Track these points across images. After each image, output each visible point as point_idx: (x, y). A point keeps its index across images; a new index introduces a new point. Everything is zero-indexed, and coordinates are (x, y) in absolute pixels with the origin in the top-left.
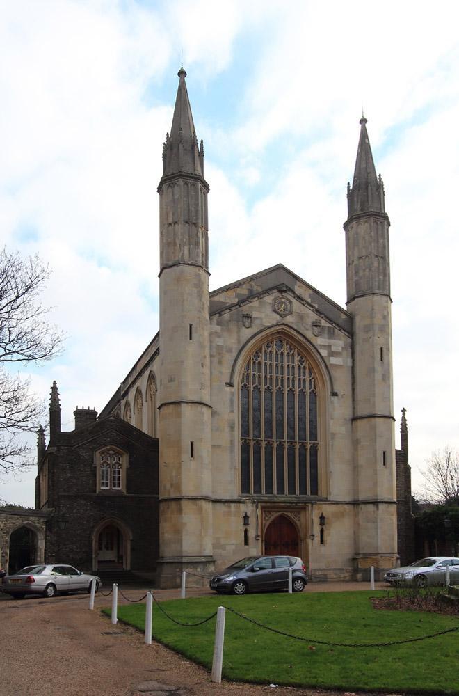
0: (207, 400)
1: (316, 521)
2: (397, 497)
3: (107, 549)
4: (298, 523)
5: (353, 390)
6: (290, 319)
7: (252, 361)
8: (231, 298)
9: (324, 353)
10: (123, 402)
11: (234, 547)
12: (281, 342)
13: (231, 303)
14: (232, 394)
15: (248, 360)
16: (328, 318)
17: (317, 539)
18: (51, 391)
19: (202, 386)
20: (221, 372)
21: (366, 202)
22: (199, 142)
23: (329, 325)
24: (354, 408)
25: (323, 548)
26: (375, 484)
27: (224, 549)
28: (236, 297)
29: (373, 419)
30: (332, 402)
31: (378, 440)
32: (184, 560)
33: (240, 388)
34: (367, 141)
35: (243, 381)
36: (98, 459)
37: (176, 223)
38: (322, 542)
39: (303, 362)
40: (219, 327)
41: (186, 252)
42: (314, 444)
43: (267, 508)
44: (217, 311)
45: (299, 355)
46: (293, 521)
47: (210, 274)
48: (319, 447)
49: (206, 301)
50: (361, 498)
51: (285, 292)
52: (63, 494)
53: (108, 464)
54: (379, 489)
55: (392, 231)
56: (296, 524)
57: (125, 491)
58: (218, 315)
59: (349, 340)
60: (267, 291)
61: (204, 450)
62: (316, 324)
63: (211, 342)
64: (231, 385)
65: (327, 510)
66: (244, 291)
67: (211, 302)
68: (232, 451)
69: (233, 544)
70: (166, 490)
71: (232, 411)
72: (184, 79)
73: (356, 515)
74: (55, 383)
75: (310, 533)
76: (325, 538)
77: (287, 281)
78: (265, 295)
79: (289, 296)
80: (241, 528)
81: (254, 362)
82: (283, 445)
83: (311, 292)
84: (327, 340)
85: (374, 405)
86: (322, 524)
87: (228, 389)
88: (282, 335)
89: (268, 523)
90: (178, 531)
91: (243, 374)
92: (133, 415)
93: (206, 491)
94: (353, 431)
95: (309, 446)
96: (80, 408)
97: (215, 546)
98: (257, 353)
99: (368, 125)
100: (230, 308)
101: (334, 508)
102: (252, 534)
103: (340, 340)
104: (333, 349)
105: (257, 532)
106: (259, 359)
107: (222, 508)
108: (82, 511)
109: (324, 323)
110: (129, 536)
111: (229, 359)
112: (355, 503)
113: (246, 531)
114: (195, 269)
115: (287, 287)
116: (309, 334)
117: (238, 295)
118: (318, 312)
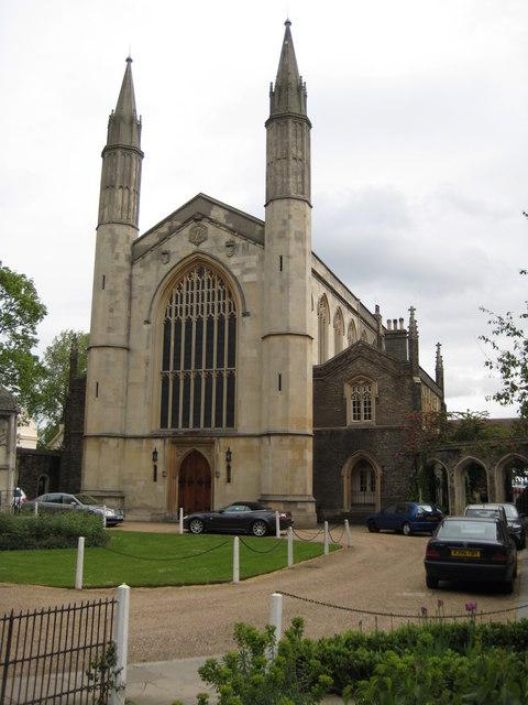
1: (222, 456)
6: (204, 247)
9: (237, 272)
17: (223, 476)
21: (288, 109)
25: (229, 486)
27: (135, 485)
30: (244, 323)
38: (229, 481)
43: (177, 441)
55: (315, 135)
60: (185, 223)
62: (230, 245)
64: (147, 322)
65: (237, 446)
66: (165, 229)
76: (234, 476)
79: (205, 223)
80: (150, 464)
83: (227, 212)
86: (228, 460)
87: (145, 327)
88: (199, 264)
99: (291, 28)
100: (151, 249)
101: (242, 442)
102: (160, 470)
104: (247, 266)
109: (238, 241)
113: (155, 467)
114: (125, 228)
116: (222, 256)
118: (232, 231)
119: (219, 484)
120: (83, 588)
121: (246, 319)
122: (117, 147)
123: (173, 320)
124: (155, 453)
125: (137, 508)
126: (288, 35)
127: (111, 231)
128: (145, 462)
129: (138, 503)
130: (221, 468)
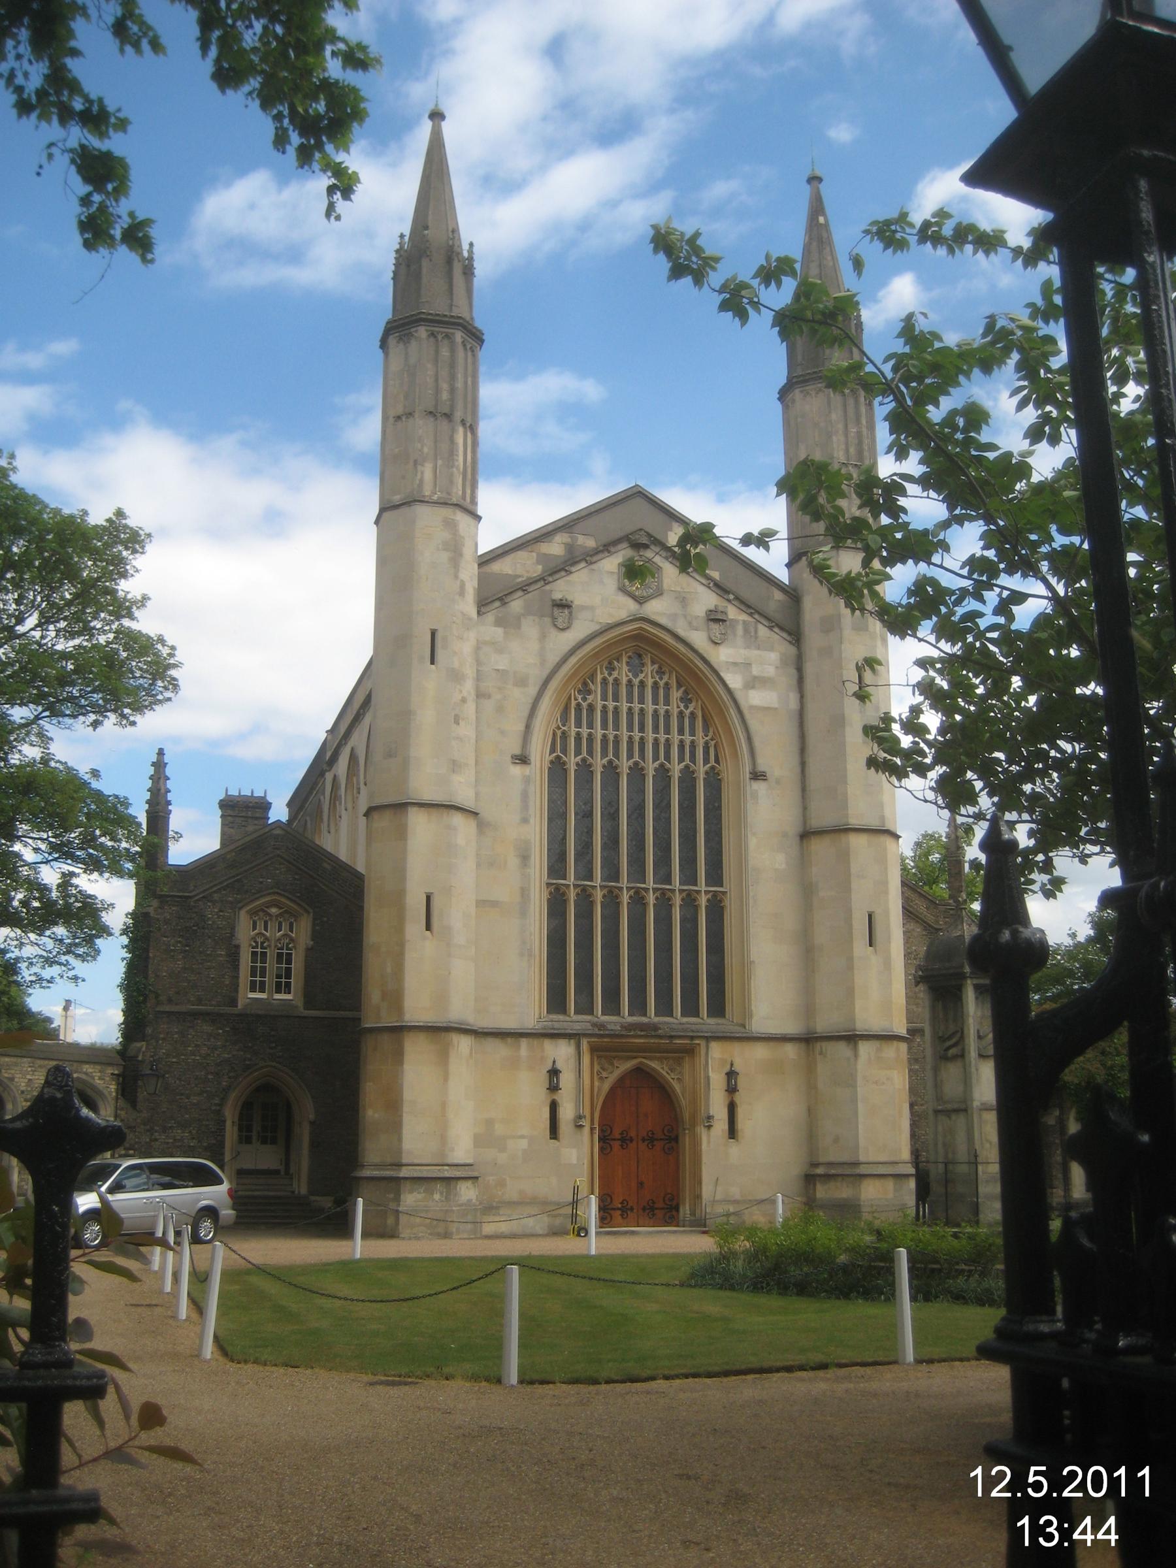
0: (464, 794)
1: (717, 1080)
2: (909, 1021)
3: (264, 1142)
4: (677, 1087)
5: (803, 764)
6: (657, 609)
7: (573, 703)
8: (525, 566)
9: (734, 681)
10: (329, 777)
11: (524, 1144)
12: (640, 656)
13: (526, 575)
14: (527, 780)
15: (564, 699)
16: (742, 602)
18: (152, 771)
19: (455, 766)
20: (503, 733)
22: (465, 247)
23: (743, 617)
24: (805, 809)
25: (735, 1151)
26: (850, 993)
28: (538, 562)
29: (843, 837)
31: (854, 885)
32: (404, 1172)
33: (547, 765)
34: (821, 220)
35: (553, 750)
36: (244, 932)
37: (410, 415)
38: (732, 1132)
39: (690, 701)
40: (500, 630)
41: (427, 472)
42: (715, 894)
43: (605, 1048)
44: (494, 596)
45: (679, 685)
46: (667, 1082)
47: (479, 518)
48: (727, 903)
49: (469, 573)
50: (822, 1025)
51: (646, 546)
52: (167, 1008)
53: (267, 939)
54: (859, 1004)
56: (674, 1091)
57: (300, 1003)
58: (497, 604)
59: (792, 650)
60: (607, 548)
61: (458, 914)
62: (715, 618)
63: (479, 662)
64: (522, 760)
65: (748, 1058)
66: (555, 548)
67: (483, 580)
68: (523, 913)
69: (522, 1137)
70: (375, 1013)
71: (525, 820)
72: (440, 127)
73: (810, 1069)
74: (161, 753)
75: (703, 1114)
77: (652, 523)
78: (600, 556)
81: (579, 705)
82: (643, 898)
84: (742, 651)
85: (844, 805)
86: (732, 1090)
87: (517, 770)
88: (641, 644)
89: (607, 1086)
90: (394, 1105)
91: (554, 734)
92: (343, 813)
93: (460, 1010)
94: (803, 862)
95: (703, 901)
96: (234, 792)
97: (479, 1141)
98: (585, 684)
100: (524, 588)
101: (760, 1052)
102: (567, 1112)
103: (772, 649)
104: (756, 671)
105: (577, 1107)
106: (590, 698)
107: (499, 1050)
108: (204, 1051)
109: (733, 613)
110: (307, 1111)
111: (521, 697)
112: (808, 1040)
113: (554, 1107)
115: (649, 535)
116: (699, 639)
117: (543, 558)
118: (720, 588)
119: (711, 1142)
120: (919, 1361)
121: (759, 787)
122: (418, 320)
123: (572, 761)
124: (554, 1073)
125: (511, 1204)
126: (817, 207)
127: (451, 525)
128: (528, 1092)
129: (512, 1191)
130: (717, 1106)
